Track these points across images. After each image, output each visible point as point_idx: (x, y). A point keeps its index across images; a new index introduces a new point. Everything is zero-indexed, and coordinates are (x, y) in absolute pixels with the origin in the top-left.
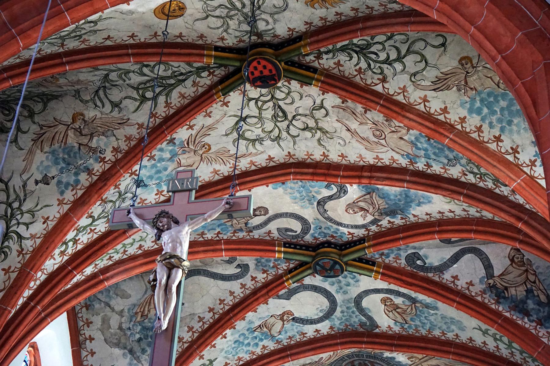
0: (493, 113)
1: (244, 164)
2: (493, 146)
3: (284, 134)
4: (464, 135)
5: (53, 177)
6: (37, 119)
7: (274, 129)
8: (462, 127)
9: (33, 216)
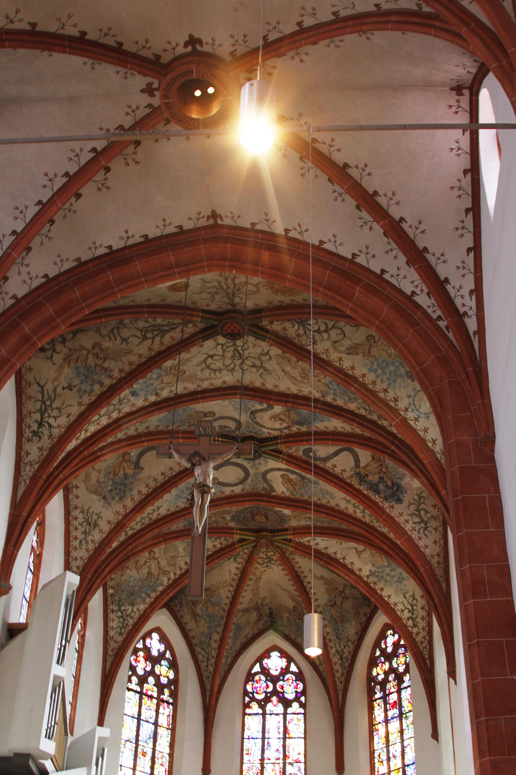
0: (385, 373)
1: (206, 385)
2: (382, 395)
3: (237, 368)
4: (363, 386)
5: (76, 386)
6: (67, 344)
7: (231, 364)
8: (363, 380)
9: (60, 412)
